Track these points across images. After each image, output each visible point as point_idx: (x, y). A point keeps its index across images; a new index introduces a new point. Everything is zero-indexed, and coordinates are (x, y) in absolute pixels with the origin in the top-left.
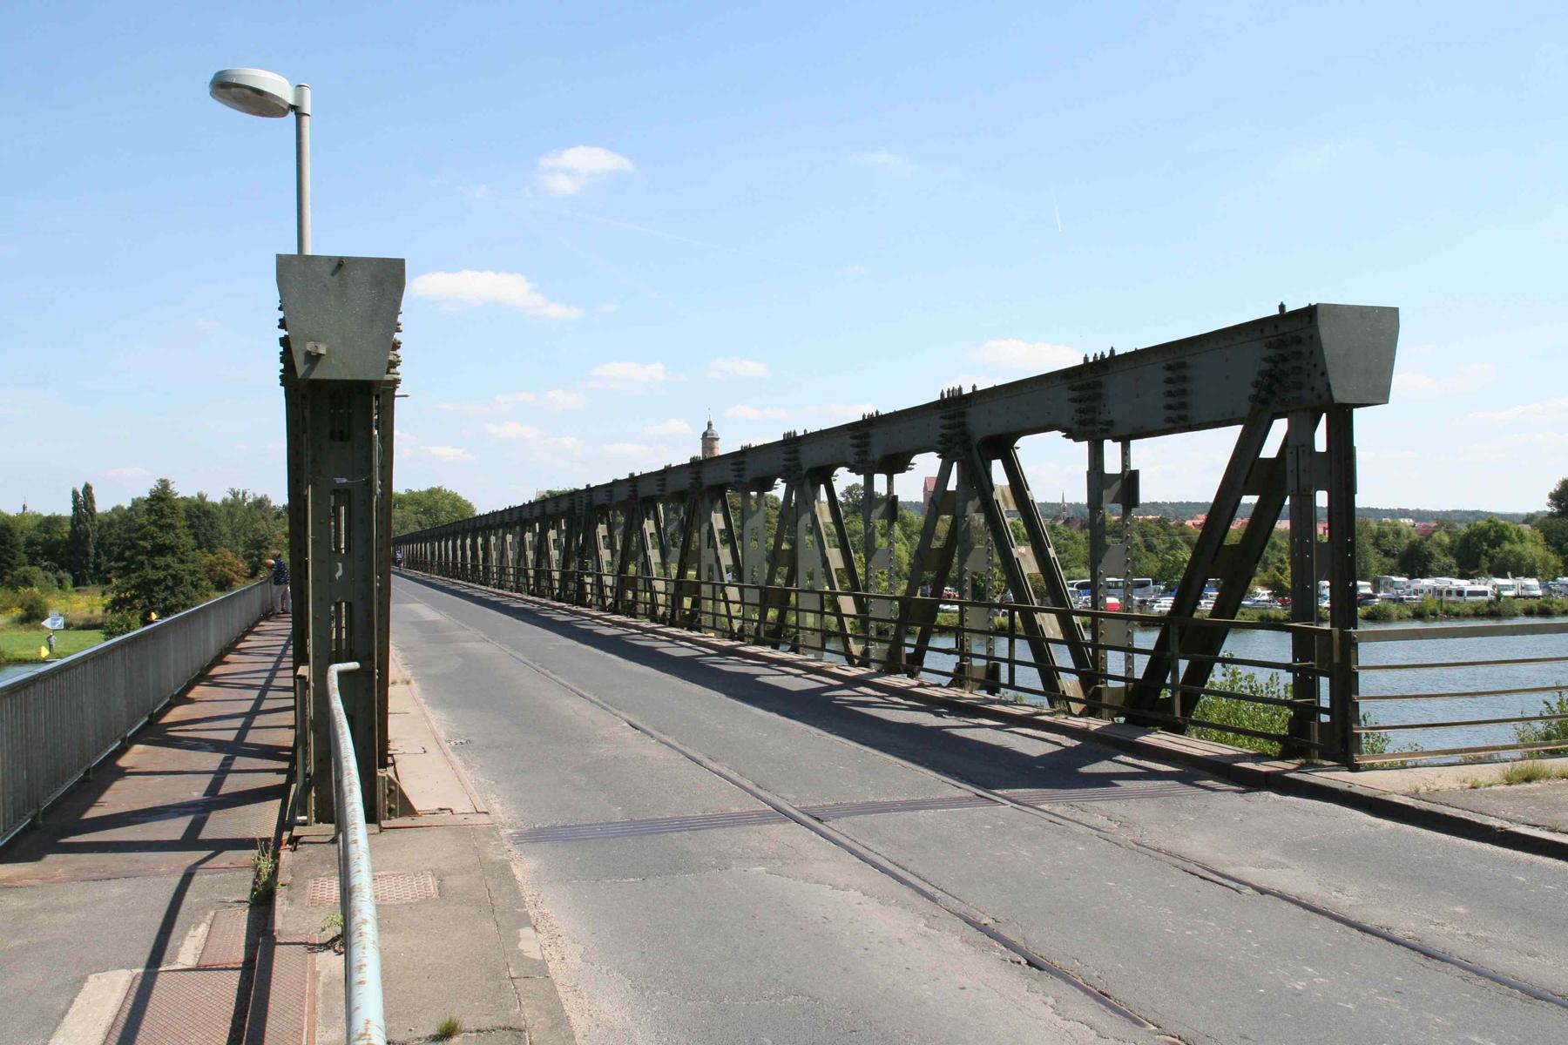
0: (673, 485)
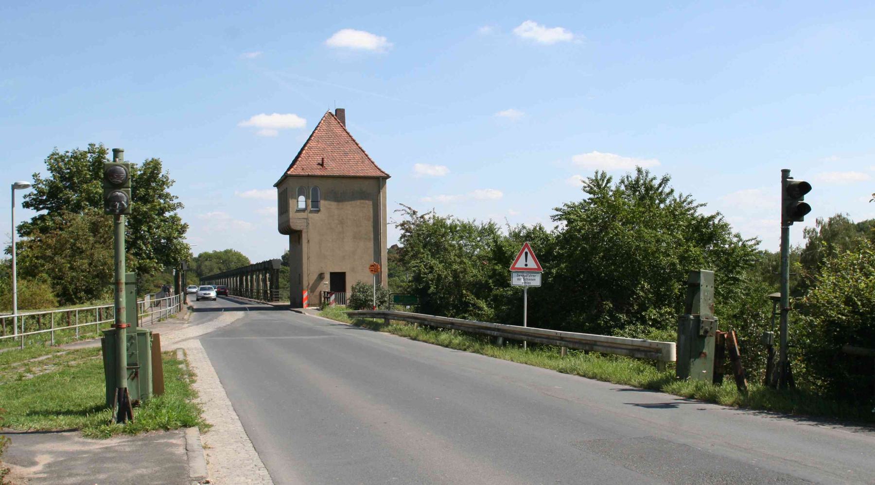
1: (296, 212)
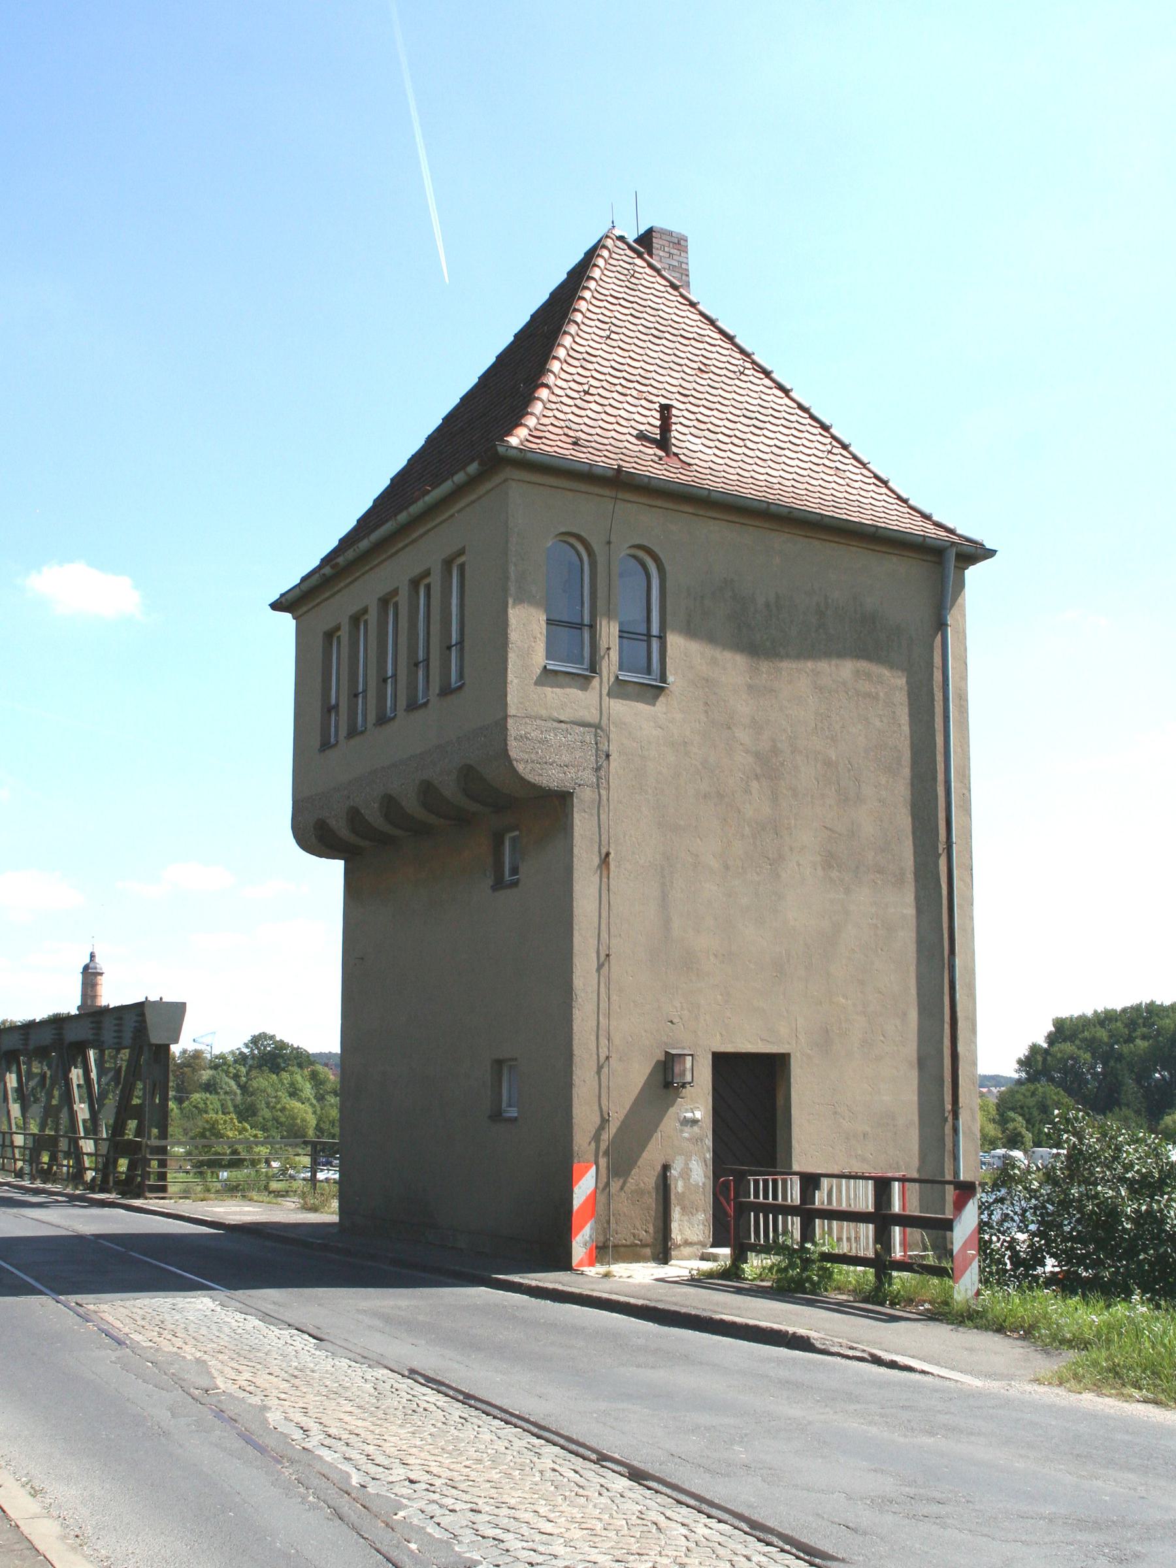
0: (36, 1040)
1: (539, 682)
